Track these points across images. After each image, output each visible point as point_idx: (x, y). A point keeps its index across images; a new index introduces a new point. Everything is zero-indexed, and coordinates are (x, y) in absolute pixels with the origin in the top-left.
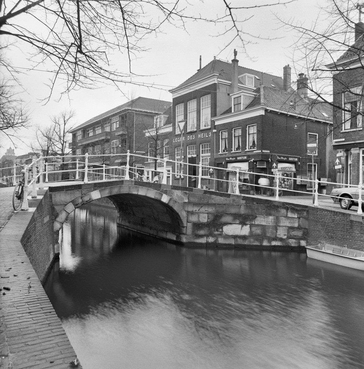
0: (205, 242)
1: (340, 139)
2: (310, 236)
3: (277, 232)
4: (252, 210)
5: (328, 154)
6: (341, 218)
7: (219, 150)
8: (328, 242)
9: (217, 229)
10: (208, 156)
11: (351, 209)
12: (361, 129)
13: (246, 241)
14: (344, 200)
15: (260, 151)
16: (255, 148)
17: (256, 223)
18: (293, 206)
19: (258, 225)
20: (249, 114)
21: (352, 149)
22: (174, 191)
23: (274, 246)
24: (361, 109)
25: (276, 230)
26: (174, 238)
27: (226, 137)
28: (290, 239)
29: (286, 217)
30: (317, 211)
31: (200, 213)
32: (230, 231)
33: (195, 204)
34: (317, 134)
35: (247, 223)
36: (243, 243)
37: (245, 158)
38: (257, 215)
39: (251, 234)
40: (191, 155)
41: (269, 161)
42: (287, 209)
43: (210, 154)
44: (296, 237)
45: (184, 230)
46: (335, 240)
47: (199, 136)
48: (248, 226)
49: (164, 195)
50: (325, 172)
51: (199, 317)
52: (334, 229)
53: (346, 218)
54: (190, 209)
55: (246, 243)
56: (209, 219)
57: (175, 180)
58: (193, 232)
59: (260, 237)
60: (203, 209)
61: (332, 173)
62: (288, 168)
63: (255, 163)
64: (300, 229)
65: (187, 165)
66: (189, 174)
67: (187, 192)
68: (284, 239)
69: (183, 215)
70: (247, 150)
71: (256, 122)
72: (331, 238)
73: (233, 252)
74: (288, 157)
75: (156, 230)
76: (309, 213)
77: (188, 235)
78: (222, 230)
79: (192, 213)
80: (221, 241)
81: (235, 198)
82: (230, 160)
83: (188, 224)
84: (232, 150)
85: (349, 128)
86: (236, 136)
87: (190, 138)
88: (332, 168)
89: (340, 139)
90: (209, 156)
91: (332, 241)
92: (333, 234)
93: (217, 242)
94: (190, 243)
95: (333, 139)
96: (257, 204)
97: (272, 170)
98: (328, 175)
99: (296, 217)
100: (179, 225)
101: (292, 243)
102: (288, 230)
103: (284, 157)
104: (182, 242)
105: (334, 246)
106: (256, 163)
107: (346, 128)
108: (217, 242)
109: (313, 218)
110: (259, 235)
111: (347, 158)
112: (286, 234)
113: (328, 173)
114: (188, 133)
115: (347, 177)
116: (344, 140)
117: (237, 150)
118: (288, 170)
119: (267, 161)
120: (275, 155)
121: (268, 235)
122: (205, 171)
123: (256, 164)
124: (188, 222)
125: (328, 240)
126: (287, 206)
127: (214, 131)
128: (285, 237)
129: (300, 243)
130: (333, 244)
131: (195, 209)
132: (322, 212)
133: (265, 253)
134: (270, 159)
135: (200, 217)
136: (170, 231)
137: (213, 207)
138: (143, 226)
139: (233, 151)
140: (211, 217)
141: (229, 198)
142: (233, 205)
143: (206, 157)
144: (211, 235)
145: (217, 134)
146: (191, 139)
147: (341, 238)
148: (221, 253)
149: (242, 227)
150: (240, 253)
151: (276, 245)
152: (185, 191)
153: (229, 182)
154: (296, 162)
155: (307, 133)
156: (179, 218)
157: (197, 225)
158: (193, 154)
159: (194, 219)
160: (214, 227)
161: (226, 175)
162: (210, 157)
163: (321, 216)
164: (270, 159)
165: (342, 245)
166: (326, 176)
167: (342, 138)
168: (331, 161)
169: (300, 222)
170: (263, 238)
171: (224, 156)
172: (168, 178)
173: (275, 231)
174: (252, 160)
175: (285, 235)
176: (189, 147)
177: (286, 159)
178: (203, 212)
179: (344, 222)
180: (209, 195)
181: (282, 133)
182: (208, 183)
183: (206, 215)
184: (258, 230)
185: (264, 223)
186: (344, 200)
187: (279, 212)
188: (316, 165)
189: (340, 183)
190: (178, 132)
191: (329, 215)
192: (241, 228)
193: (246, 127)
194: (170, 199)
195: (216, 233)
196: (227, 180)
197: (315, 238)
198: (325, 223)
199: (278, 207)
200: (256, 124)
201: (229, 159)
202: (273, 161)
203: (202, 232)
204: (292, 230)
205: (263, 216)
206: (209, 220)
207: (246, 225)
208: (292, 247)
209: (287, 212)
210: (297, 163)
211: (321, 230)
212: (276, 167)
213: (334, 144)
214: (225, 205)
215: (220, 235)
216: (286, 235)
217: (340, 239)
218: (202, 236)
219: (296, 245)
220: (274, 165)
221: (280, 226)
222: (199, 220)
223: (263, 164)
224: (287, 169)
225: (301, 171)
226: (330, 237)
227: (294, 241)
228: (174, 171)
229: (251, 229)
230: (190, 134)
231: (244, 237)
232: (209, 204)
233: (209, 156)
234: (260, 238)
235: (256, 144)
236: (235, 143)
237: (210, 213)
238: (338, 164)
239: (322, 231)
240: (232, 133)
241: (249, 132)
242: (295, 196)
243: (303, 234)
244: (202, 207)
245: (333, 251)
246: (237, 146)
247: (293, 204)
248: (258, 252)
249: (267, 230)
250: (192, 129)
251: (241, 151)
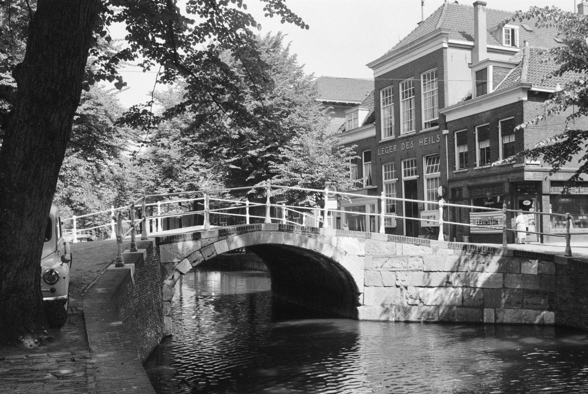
7: (455, 165)
24: (508, 139)
43: (439, 173)
47: (420, 142)
51: (418, 320)
65: (402, 202)
84: (475, 166)
124: (365, 286)
127: (445, 132)
146: (407, 148)
172: (372, 218)
190: (384, 138)
240: (475, 134)
250: (408, 238)
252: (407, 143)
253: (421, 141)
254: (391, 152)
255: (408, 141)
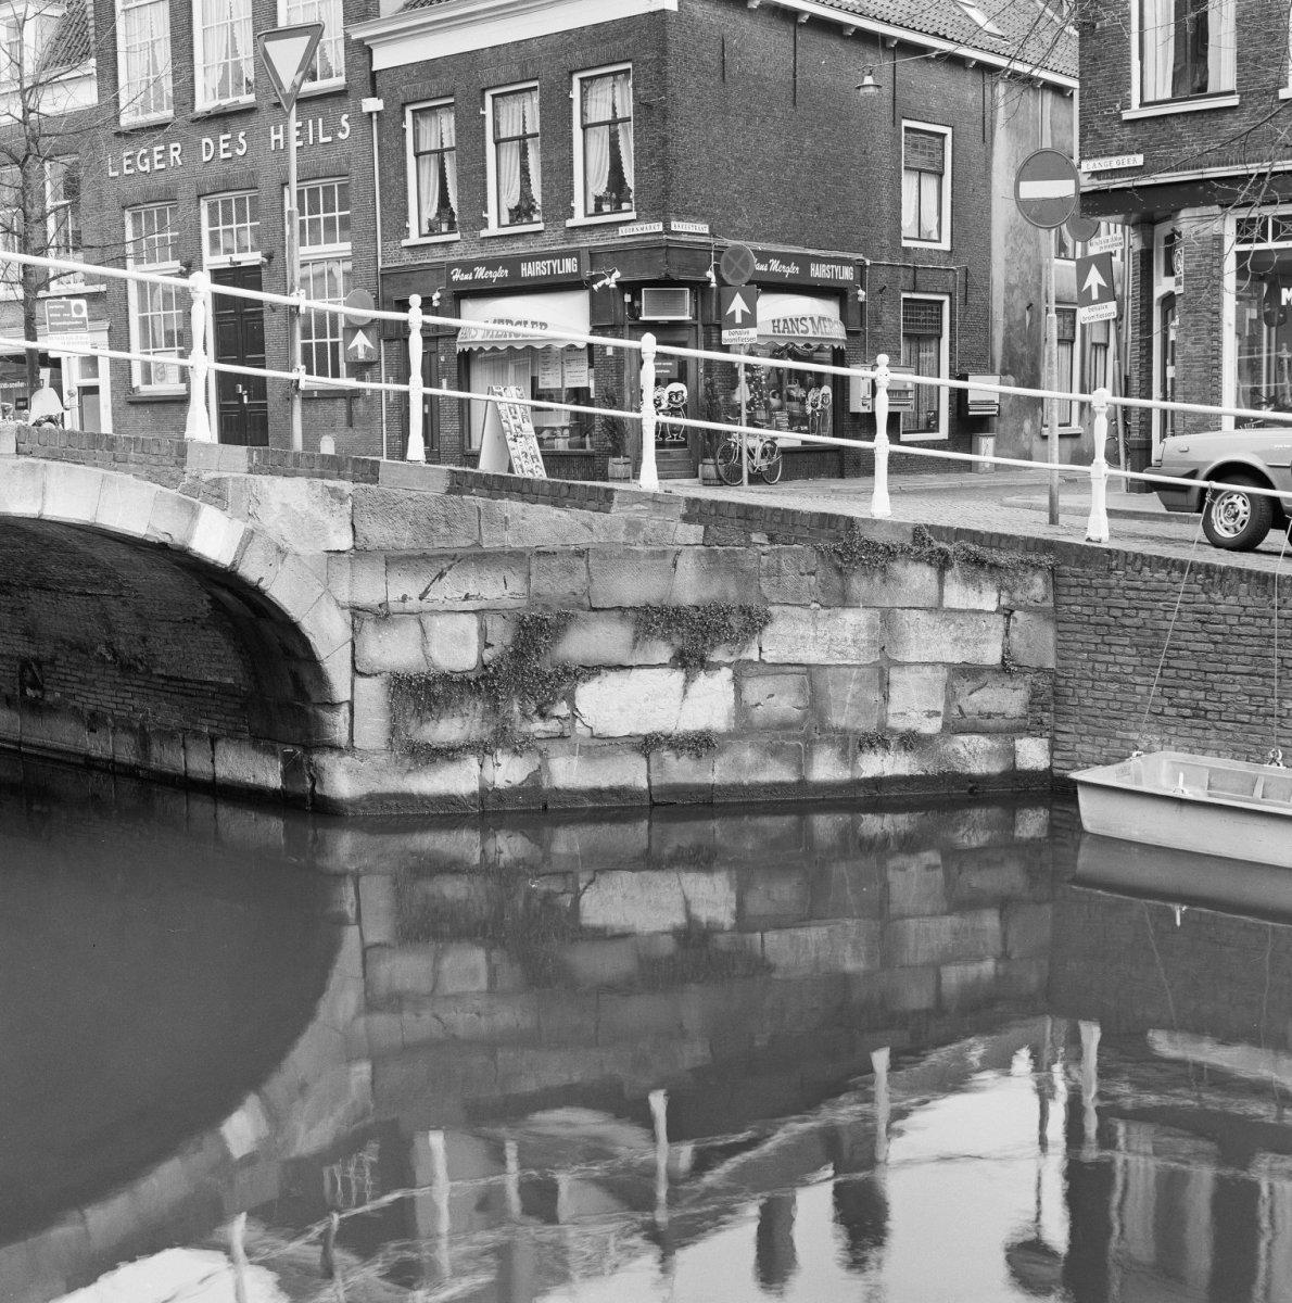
0: (474, 786)
1: (1117, 155)
2: (1072, 710)
3: (886, 698)
4: (747, 578)
5: (1002, 239)
6: (1248, 601)
7: (407, 219)
8: (1176, 741)
9: (539, 708)
10: (337, 260)
11: (1260, 547)
12: (1234, 101)
13: (717, 767)
14: (1226, 501)
15: (659, 227)
16: (625, 206)
17: (770, 656)
18: (972, 548)
19: (779, 668)
20: (431, 38)
21: (1184, 214)
22: (264, 481)
23: (878, 782)
25: (885, 685)
26: (268, 774)
27: (446, 146)
28: (964, 732)
29: (937, 608)
30: (1111, 570)
31: (436, 612)
32: (621, 710)
33: (395, 561)
34: (948, 131)
35: (718, 655)
36: (698, 779)
37: (570, 266)
38: (774, 610)
39: (745, 725)
40: (228, 251)
41: (709, 282)
42: (942, 563)
43: (348, 246)
44: (990, 723)
45: (339, 731)
46: (1218, 724)
47: (274, 137)
48: (726, 674)
49: (209, 514)
50: (989, 341)
52: (1208, 666)
53: (1276, 600)
54: (371, 588)
55: (716, 773)
56: (488, 645)
57: (132, 410)
58: (393, 731)
59: (797, 737)
60: (449, 590)
61: (1021, 349)
62: (809, 323)
63: (628, 298)
64: (1010, 673)
66: (953, 376)
67: (347, 486)
68: (931, 738)
69: (326, 632)
70: (579, 219)
71: (629, 54)
72: (1195, 716)
73: (637, 834)
74: (804, 261)
75: (131, 730)
76: (1061, 581)
77: (365, 754)
78: (574, 708)
79: (383, 615)
80: (568, 773)
81: (637, 511)
82: (474, 280)
83: (361, 682)
84: (484, 223)
85: (1168, 95)
86: (503, 136)
87: (215, 147)
88: (1018, 317)
89: (1120, 158)
90: (345, 259)
91: (1199, 733)
92: (1201, 695)
93: (546, 786)
94: (373, 798)
95: (1082, 158)
96: (772, 539)
97: (725, 334)
98: (1004, 358)
99: (993, 607)
100: (306, 697)
101: (976, 756)
102: (949, 686)
103: (785, 259)
104: (324, 798)
105: (1210, 761)
106: (636, 296)
107: (1149, 98)
108: (546, 786)
109: (1087, 611)
110: (785, 725)
111: (1145, 260)
112: (940, 707)
113: (1005, 351)
114: (198, 119)
115: (1150, 370)
116: (1138, 160)
117: (512, 223)
118: (810, 334)
119: (698, 282)
120: (738, 252)
121: (839, 719)
122: (321, 347)
123: (631, 304)
124: (356, 671)
125: (1173, 730)
126: (943, 545)
127: (372, 105)
128: (932, 727)
129: (1012, 752)
130: (1204, 750)
131: (403, 588)
132: (1139, 572)
133: (824, 825)
134: (710, 274)
135: (435, 638)
136: (234, 735)
137: (507, 573)
138: (36, 708)
139: (493, 229)
140: (501, 634)
141: (607, 516)
142: (629, 554)
143: (325, 267)
144: (501, 740)
145: (389, 123)
146: (223, 156)
147: (1251, 714)
148: (567, 841)
149: (688, 680)
150: (682, 835)
151: (889, 773)
152: (331, 483)
153: (473, 403)
154: (843, 285)
155: (895, 123)
156: (301, 654)
157: (420, 686)
158: (243, 249)
159: (395, 650)
160: (525, 692)
161: (454, 370)
162: (348, 266)
163: (1132, 594)
164: (710, 274)
165: (1258, 755)
166: (993, 363)
167: (1132, 153)
168: (1013, 280)
169: (1014, 635)
170: (814, 741)
171: (438, 256)
173: (879, 697)
174: (611, 282)
175: (932, 714)
176: (213, 208)
177: (793, 269)
178: (449, 605)
179: (1265, 622)
180: (480, 501)
181: (769, 120)
182: (344, 419)
183: (470, 624)
184: (782, 693)
185: (813, 656)
186: (1226, 501)
187: (898, 581)
188: (941, 302)
189: (1126, 395)
191: (1182, 587)
192: (685, 692)
193: (403, 112)
194: (249, 537)
195: (538, 727)
196: (461, 389)
197: (1101, 721)
198: (1156, 632)
199: (890, 553)
200: (629, 66)
201: (468, 277)
202: (730, 282)
203: (447, 730)
204: (969, 685)
205: (805, 613)
206: (488, 655)
207: (705, 665)
208: (971, 778)
209: (941, 582)
210: (851, 294)
211: (1135, 672)
212: (750, 320)
213: (1089, 185)
214: (580, 554)
215: (562, 737)
216: (937, 714)
217: (1245, 718)
218: (447, 754)
219: (996, 767)
220: (738, 305)
221: (902, 665)
222: (427, 657)
223: (673, 303)
224: (802, 328)
225: (873, 336)
226: (1187, 712)
227: (982, 742)
228: (119, 339)
229: (739, 690)
230: (214, 126)
231: (700, 744)
232: (484, 556)
233: (345, 259)
234: (793, 743)
235: (630, 182)
236: (502, 188)
237: (495, 611)
238: (1095, 296)
239: (1139, 680)
240: (484, 116)
241: (583, 114)
242: (842, 476)
243: (1031, 703)
244: (441, 575)
245: (1210, 787)
246: (512, 198)
247: (974, 536)
248: (786, 822)
249: (831, 690)
251: (540, 227)
252: (223, 137)
253: (277, 132)
254: (157, 167)
255: (226, 133)
